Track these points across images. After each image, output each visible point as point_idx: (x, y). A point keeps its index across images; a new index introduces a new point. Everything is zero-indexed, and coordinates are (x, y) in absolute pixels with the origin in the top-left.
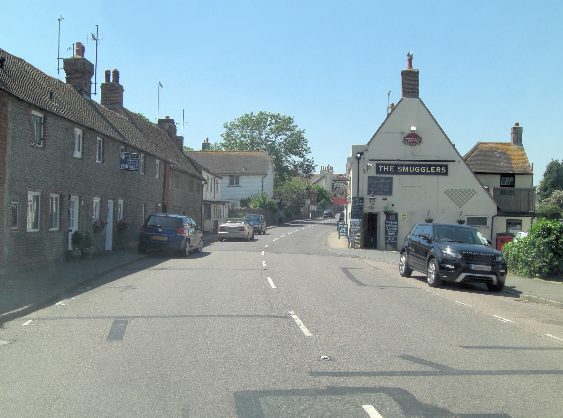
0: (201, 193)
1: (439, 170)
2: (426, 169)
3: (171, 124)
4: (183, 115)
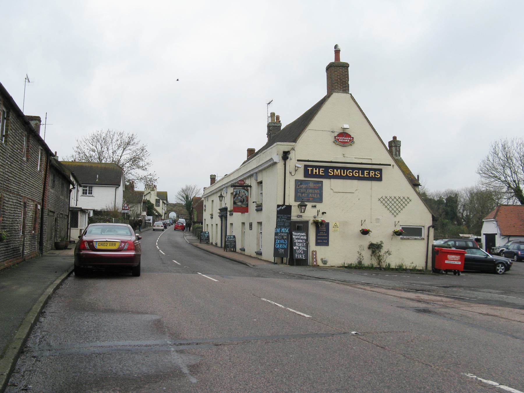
0: (69, 198)
1: (373, 174)
2: (359, 173)
3: (38, 122)
4: (46, 118)
